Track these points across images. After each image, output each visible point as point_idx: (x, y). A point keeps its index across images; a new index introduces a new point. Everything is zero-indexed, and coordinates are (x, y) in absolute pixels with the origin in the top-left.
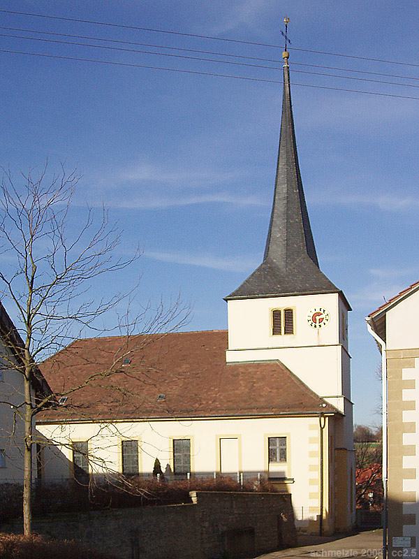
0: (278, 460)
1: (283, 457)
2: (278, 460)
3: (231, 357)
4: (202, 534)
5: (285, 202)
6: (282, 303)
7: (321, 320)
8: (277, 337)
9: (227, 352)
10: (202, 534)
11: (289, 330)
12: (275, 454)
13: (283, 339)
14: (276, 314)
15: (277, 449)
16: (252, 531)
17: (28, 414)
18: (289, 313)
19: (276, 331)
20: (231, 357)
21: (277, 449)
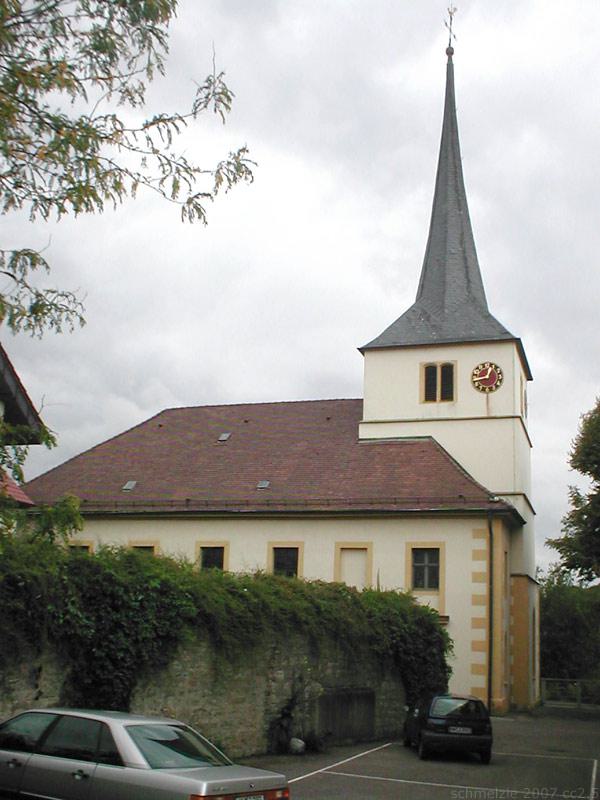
0: (488, 738)
1: (434, 584)
2: (488, 738)
3: (365, 432)
4: (268, 693)
5: (554, 569)
6: (439, 357)
7: (484, 373)
8: (431, 405)
9: (361, 426)
10: (268, 693)
11: (448, 395)
12: (422, 576)
13: (439, 408)
14: (430, 371)
15: (426, 566)
16: (82, 196)
17: (207, 722)
18: (448, 370)
19: (430, 396)
20: (365, 432)
21: (426, 566)
